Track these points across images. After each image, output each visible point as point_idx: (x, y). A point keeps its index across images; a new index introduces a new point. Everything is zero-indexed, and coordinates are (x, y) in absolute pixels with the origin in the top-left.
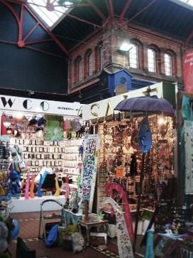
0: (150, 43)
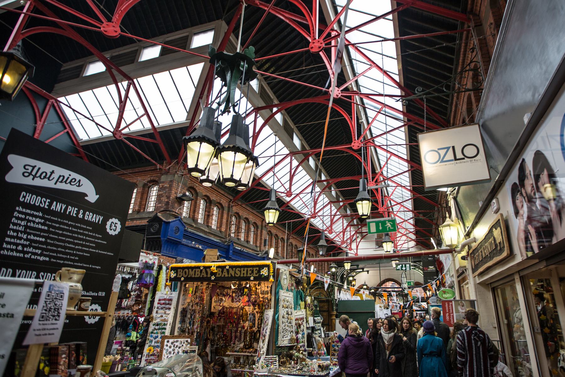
0: (204, 194)
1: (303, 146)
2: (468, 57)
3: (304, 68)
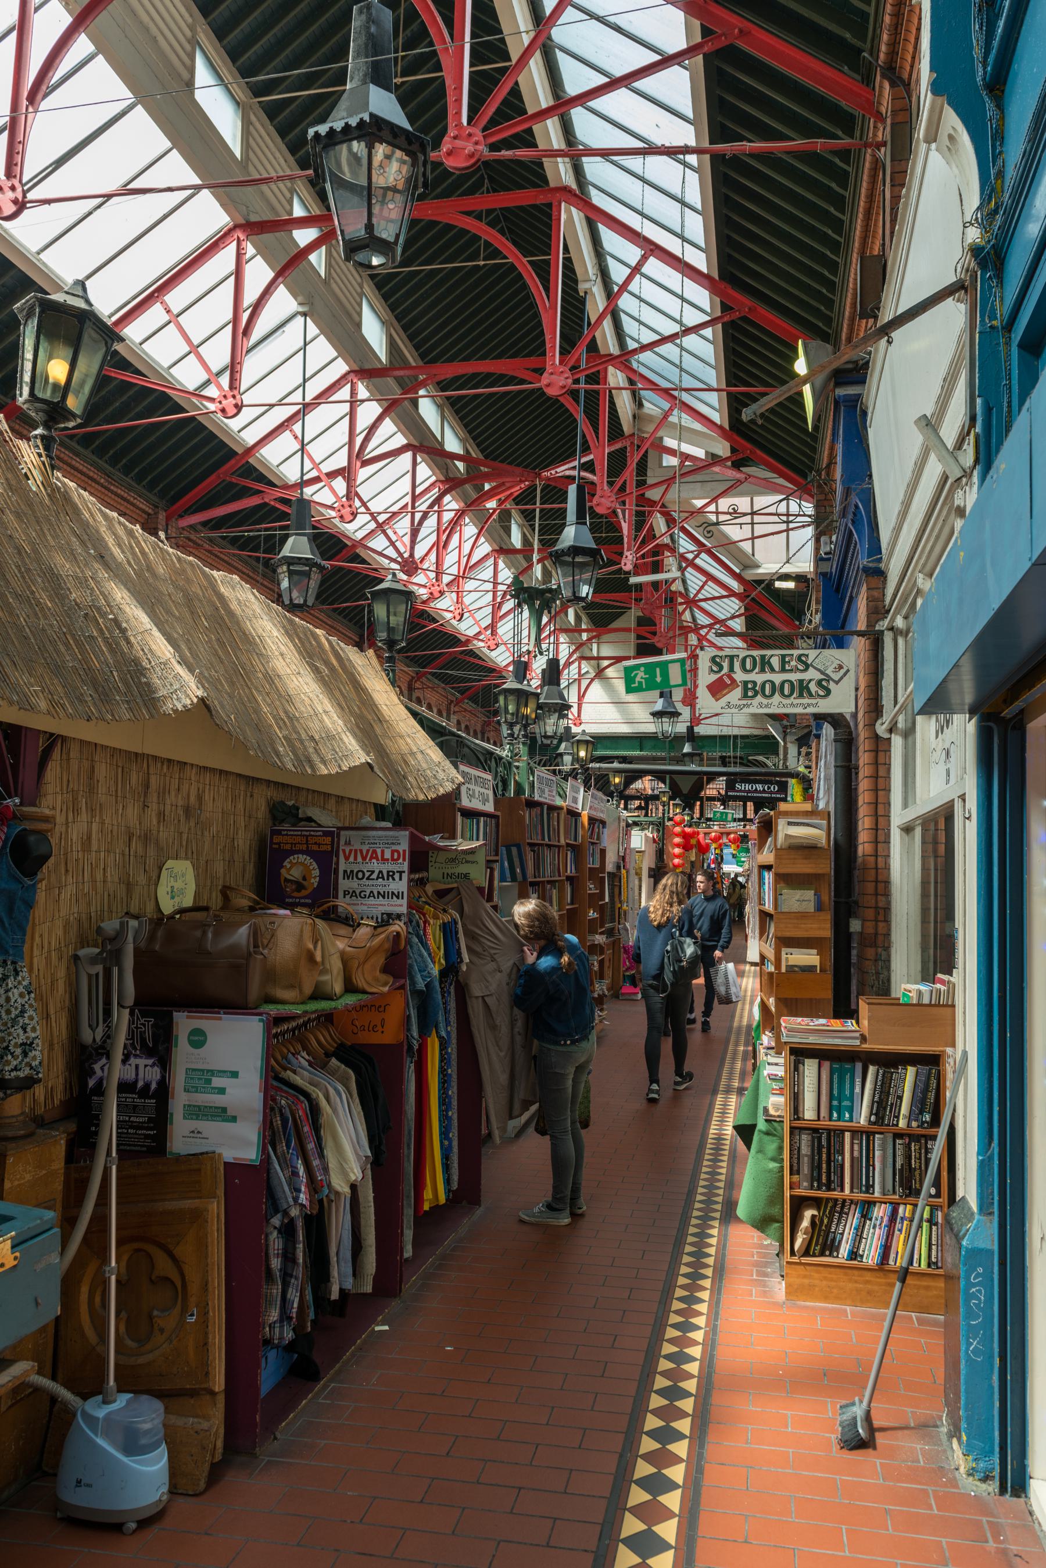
1: (392, 346)
2: (905, 40)
3: (482, 263)
